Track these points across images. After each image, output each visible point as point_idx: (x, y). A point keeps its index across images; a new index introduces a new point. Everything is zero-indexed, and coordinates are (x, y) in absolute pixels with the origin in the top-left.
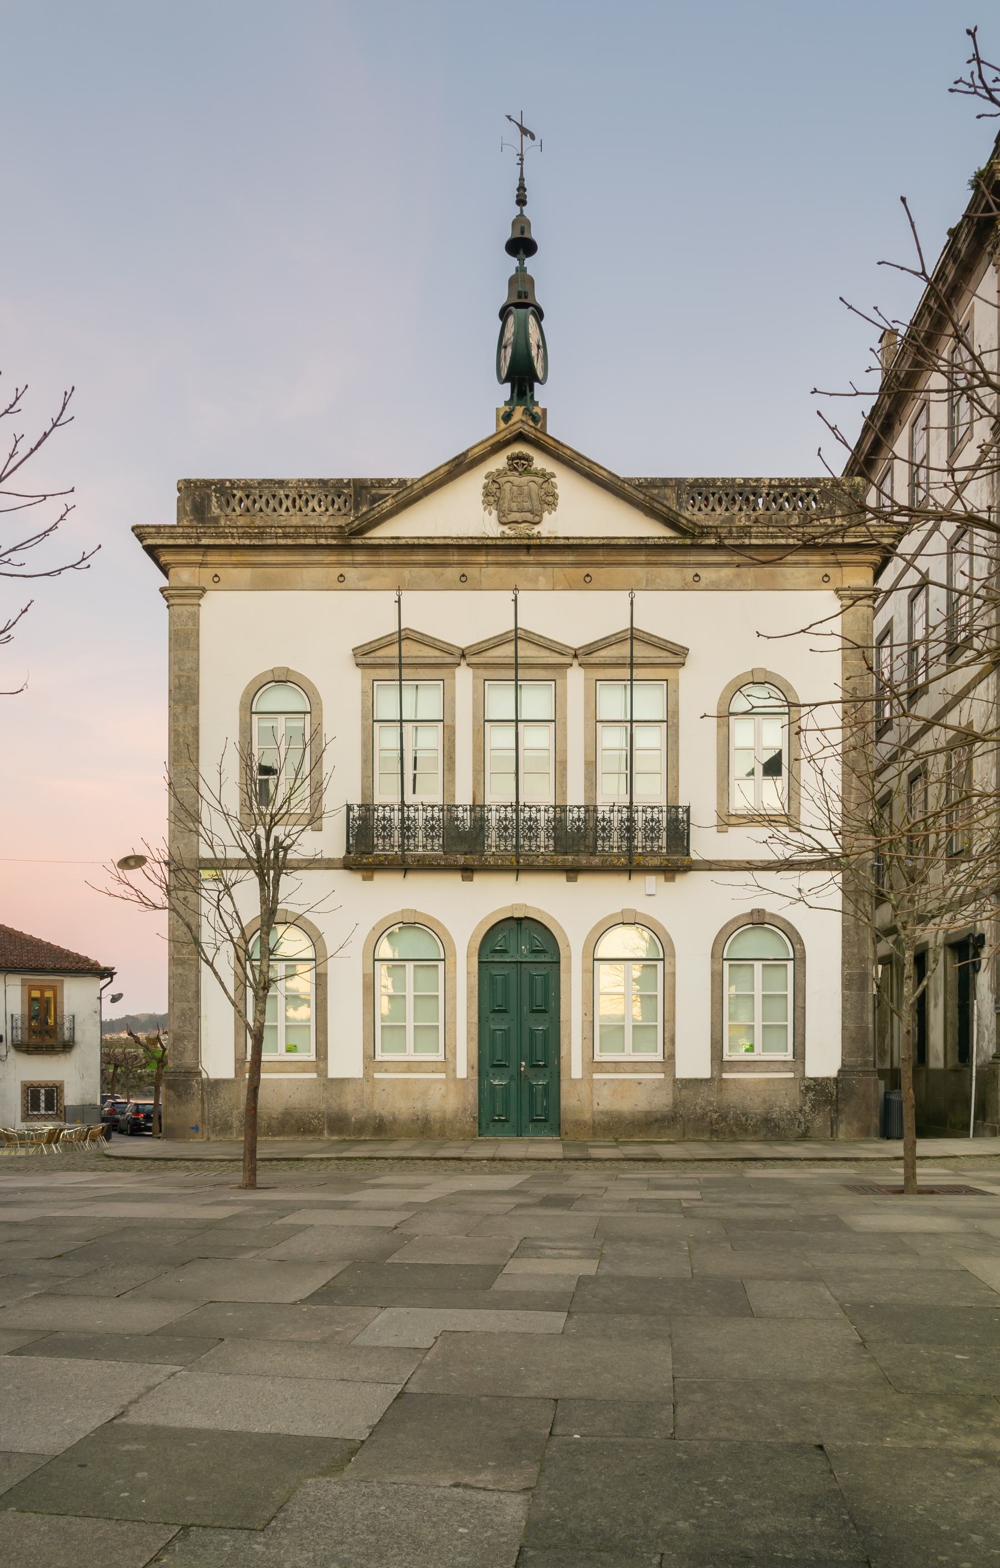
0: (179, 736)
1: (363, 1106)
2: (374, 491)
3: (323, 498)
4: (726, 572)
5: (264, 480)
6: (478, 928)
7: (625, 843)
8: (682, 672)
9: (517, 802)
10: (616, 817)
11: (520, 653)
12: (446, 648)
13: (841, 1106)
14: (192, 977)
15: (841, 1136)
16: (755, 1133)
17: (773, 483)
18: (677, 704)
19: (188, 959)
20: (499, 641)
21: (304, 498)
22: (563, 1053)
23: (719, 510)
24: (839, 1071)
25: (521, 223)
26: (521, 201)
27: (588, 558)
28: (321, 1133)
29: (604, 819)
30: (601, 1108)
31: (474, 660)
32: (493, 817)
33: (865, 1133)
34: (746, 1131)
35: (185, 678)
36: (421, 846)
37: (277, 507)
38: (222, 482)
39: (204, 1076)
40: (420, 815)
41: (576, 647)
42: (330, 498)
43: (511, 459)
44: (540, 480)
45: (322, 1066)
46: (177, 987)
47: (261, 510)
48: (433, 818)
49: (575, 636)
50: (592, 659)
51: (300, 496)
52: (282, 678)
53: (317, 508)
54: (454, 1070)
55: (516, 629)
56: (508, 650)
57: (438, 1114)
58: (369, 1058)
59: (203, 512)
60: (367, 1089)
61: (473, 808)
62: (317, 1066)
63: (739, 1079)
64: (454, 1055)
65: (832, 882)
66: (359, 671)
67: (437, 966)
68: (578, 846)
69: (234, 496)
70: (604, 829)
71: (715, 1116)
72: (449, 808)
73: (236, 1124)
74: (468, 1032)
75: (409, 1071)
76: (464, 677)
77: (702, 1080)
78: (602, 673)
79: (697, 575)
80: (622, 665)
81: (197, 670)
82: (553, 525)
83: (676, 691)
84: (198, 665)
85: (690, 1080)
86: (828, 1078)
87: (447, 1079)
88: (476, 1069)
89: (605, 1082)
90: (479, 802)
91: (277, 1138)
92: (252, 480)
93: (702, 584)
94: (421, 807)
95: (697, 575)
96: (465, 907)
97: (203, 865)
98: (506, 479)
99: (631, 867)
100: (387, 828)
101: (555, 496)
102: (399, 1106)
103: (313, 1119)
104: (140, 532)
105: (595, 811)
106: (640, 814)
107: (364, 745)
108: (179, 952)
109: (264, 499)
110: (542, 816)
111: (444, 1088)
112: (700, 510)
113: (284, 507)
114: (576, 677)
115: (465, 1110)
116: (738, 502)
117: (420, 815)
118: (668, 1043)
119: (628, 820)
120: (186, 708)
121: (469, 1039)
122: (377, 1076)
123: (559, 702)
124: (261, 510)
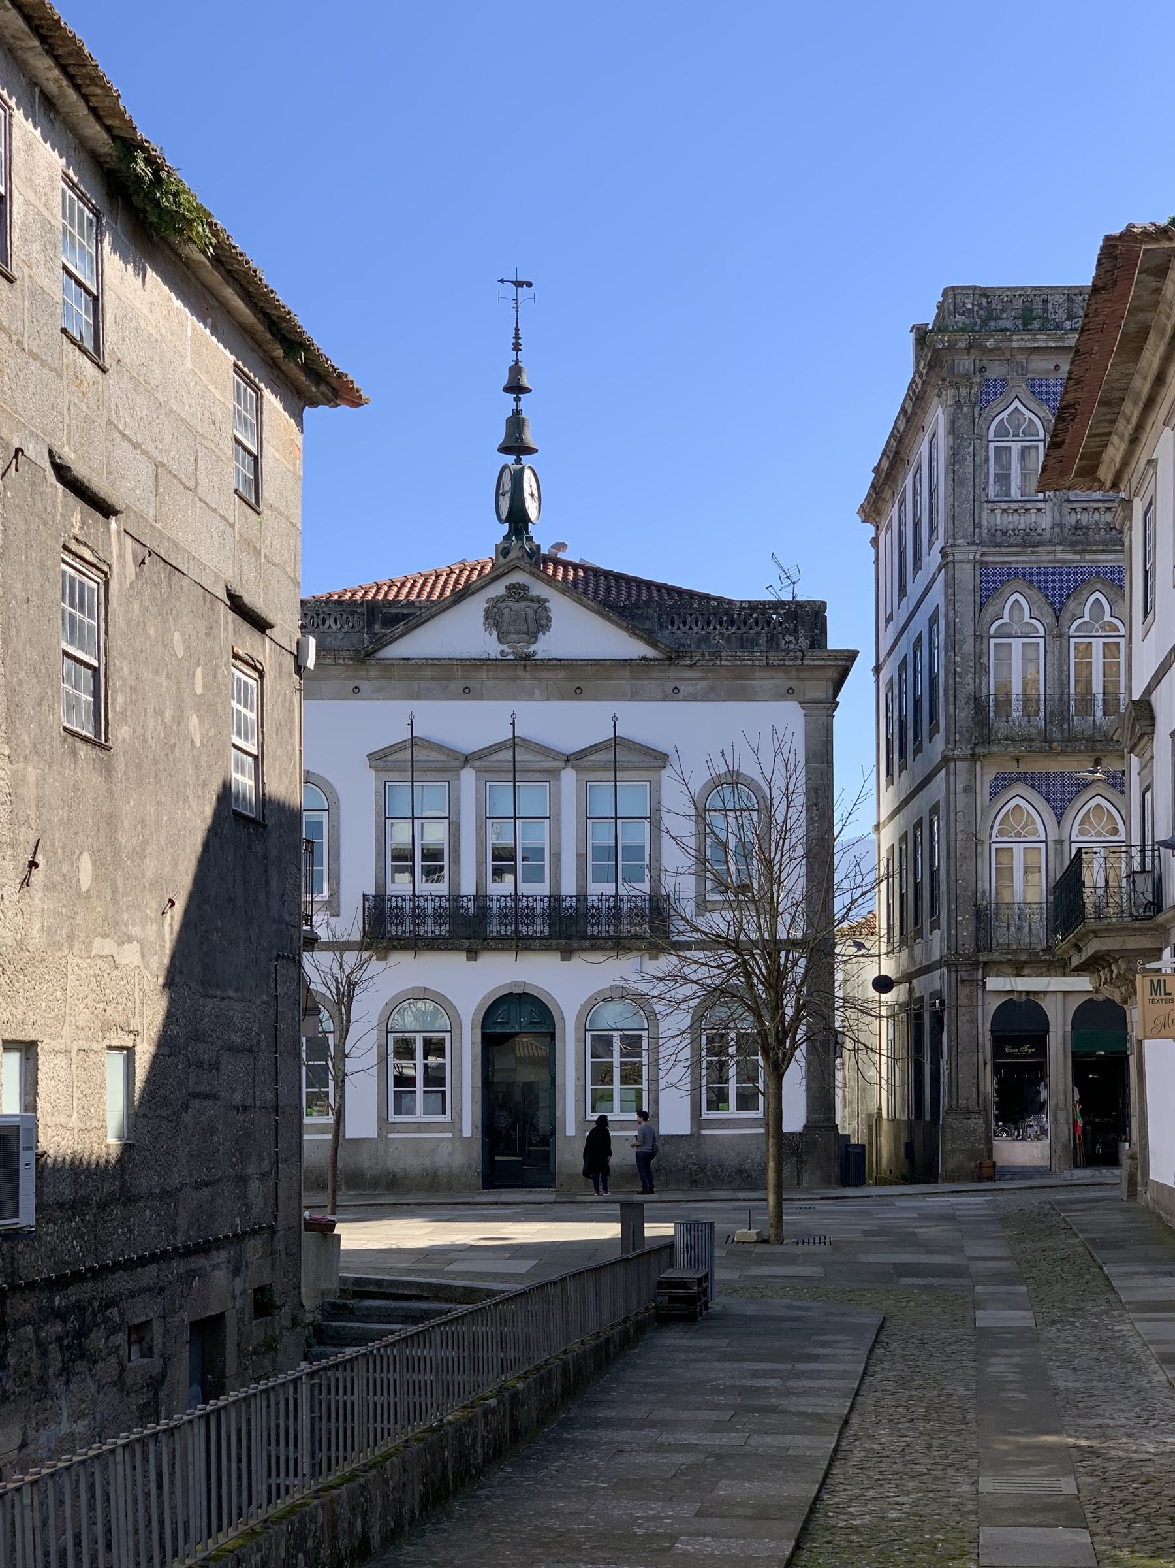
2: (385, 610)
4: (702, 685)
6: (481, 1004)
8: (664, 773)
9: (516, 894)
10: (604, 906)
11: (518, 758)
12: (452, 753)
13: (805, 1157)
15: (805, 1185)
16: (730, 1182)
21: (321, 616)
22: (558, 1114)
24: (805, 1127)
25: (516, 370)
26: (517, 348)
27: (579, 678)
29: (593, 907)
31: (477, 764)
33: (827, 1182)
34: (722, 1180)
36: (429, 929)
40: (429, 906)
42: (344, 617)
43: (508, 588)
44: (535, 605)
48: (440, 907)
50: (581, 764)
51: (318, 615)
53: (333, 626)
54: (461, 1130)
56: (507, 755)
58: (383, 1120)
61: (476, 898)
66: (373, 772)
67: (444, 1112)
70: (593, 916)
72: (455, 898)
74: (473, 1096)
76: (468, 777)
78: (590, 777)
82: (546, 646)
83: (658, 791)
85: (672, 1136)
90: (482, 893)
93: (681, 695)
96: (468, 984)
99: (618, 944)
101: (549, 619)
102: (411, 1163)
110: (538, 906)
111: (451, 1147)
114: (569, 777)
115: (470, 1166)
117: (429, 906)
118: (652, 1103)
121: (474, 1102)
122: (391, 1136)
123: (554, 800)
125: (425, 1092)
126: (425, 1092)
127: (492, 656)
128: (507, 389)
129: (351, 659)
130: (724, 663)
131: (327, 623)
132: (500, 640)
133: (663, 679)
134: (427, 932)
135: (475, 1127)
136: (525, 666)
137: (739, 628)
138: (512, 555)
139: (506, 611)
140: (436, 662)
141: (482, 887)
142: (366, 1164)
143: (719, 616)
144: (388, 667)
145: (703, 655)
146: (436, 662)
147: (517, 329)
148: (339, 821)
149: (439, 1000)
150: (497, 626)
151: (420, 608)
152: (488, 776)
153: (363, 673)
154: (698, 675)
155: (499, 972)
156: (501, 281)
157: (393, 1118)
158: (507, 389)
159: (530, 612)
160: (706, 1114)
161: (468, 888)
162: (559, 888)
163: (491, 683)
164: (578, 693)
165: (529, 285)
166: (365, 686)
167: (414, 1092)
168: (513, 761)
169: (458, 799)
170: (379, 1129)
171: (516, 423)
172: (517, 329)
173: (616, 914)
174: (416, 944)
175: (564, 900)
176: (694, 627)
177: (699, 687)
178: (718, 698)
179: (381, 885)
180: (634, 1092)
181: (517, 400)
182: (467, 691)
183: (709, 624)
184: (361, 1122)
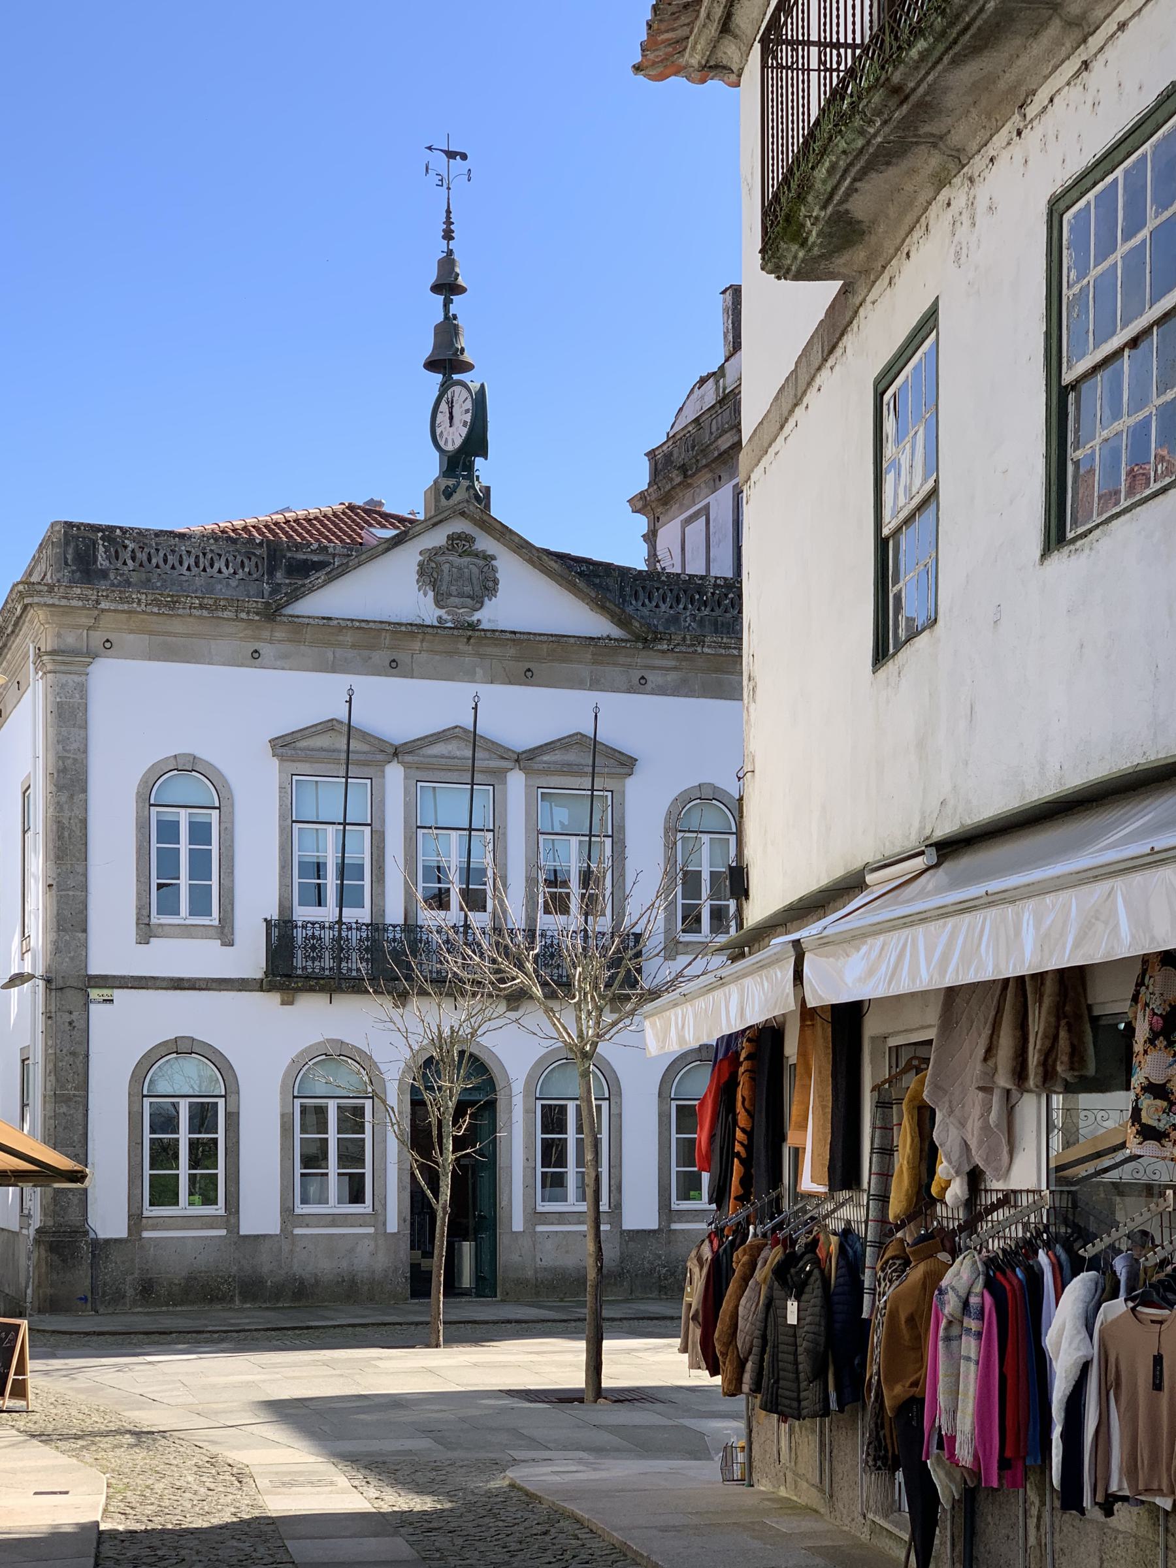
0: (63, 828)
2: (289, 555)
3: (231, 558)
4: (672, 677)
5: (161, 531)
8: (630, 782)
14: (80, 1116)
17: (718, 581)
18: (623, 818)
19: (74, 1095)
21: (209, 556)
25: (447, 263)
26: (448, 235)
27: (531, 658)
28: (232, 1300)
30: (544, 1263)
34: (885, 1235)
35: (69, 761)
37: (177, 564)
38: (112, 529)
39: (92, 1235)
41: (520, 750)
42: (239, 559)
44: (481, 563)
45: (233, 1221)
46: (60, 1129)
47: (157, 566)
49: (523, 738)
51: (204, 554)
52: (187, 766)
53: (224, 569)
54: (385, 1224)
57: (366, 1275)
58: (287, 1212)
59: (88, 564)
60: (286, 1247)
62: (228, 1221)
63: (688, 1230)
64: (384, 1206)
66: (276, 761)
69: (126, 547)
73: (130, 1292)
75: (333, 1224)
79: (643, 678)
80: (581, 774)
81: (85, 751)
84: (86, 745)
85: (638, 1231)
87: (376, 1233)
88: (408, 1222)
89: (549, 1235)
91: (179, 1308)
92: (147, 530)
94: (354, 926)
95: (643, 678)
96: (387, 1036)
97: (92, 984)
101: (496, 582)
102: (324, 1266)
103: (222, 1284)
106: (300, 930)
107: (282, 849)
108: (63, 1087)
109: (161, 554)
111: (372, 1243)
113: (186, 565)
114: (516, 781)
115: (396, 1269)
116: (683, 600)
120: (72, 796)
121: (401, 1189)
122: (297, 1231)
123: (378, 804)
124: (157, 566)
125: (339, 1174)
126: (302, 1175)
127: (428, 622)
128: (436, 289)
129: (257, 614)
130: (706, 650)
131: (216, 566)
132: (438, 603)
133: (630, 666)
134: (323, 969)
135: (402, 1219)
136: (469, 638)
137: (712, 610)
138: (457, 497)
139: (446, 567)
140: (363, 625)
141: (411, 915)
142: (265, 1269)
143: (690, 593)
144: (299, 626)
145: (684, 639)
146: (363, 625)
147: (448, 212)
148: (233, 823)
149: (364, 1060)
150: (434, 585)
151: (334, 555)
152: (420, 775)
153: (266, 634)
154: (673, 663)
155: (428, 1020)
156: (430, 148)
157: (301, 1209)
158: (436, 289)
159: (475, 570)
160: (677, 1205)
161: (394, 914)
162: (383, 916)
163: (424, 656)
164: (528, 677)
165: (464, 157)
166: (266, 649)
167: (327, 1174)
168: (471, 758)
169: (383, 802)
170: (283, 1222)
171: (448, 330)
172: (448, 212)
173: (340, 948)
174: (335, 984)
175: (385, 930)
176: (661, 604)
177: (669, 678)
178: (691, 694)
179: (285, 907)
181: (447, 304)
182: (394, 664)
183: (678, 602)
184: (260, 1214)
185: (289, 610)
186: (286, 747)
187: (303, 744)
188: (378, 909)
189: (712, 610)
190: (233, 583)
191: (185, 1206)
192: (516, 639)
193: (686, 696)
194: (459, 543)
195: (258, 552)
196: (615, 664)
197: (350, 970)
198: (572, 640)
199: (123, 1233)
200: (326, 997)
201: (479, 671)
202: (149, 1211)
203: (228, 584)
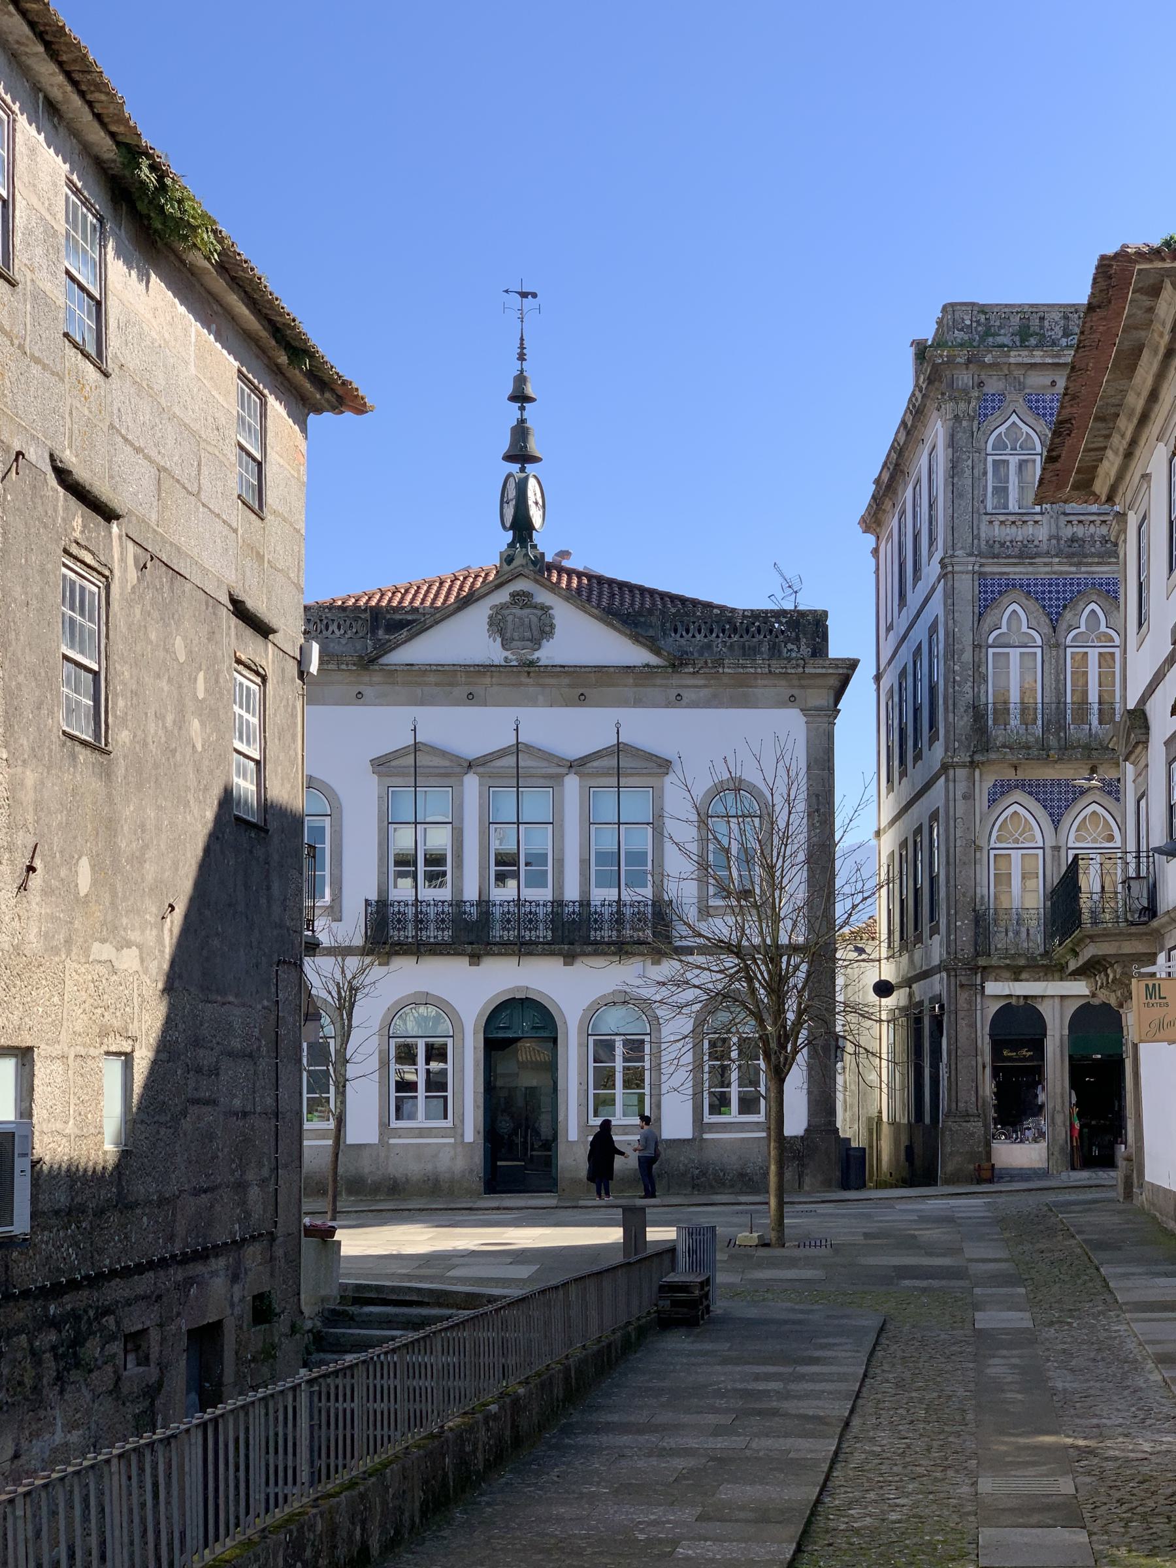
1: (378, 1169)
2: (388, 616)
6: (483, 1009)
7: (614, 933)
8: (668, 779)
10: (606, 911)
12: (455, 758)
15: (806, 1188)
16: (732, 1186)
20: (502, 753)
23: (698, 636)
25: (521, 380)
26: (522, 357)
27: (583, 684)
29: (596, 913)
31: (481, 770)
32: (497, 911)
33: (828, 1185)
34: (724, 1184)
36: (431, 934)
40: (432, 911)
41: (471, 758)
42: (348, 623)
43: (513, 595)
44: (539, 613)
48: (443, 913)
49: (575, 750)
53: (336, 631)
54: (463, 1136)
55: (518, 743)
58: (384, 1125)
60: (383, 1155)
61: (479, 903)
65: (866, 895)
66: (375, 777)
68: (572, 933)
70: (596, 921)
71: (697, 1172)
74: (475, 1101)
76: (471, 783)
77: (684, 1140)
80: (408, 775)
82: (550, 653)
85: (674, 1140)
86: (796, 1137)
96: (472, 988)
98: (508, 611)
99: (621, 949)
100: (401, 921)
101: (552, 626)
102: (413, 1168)
104: (366, 900)
105: (589, 904)
110: (541, 911)
111: (452, 1153)
112: (682, 636)
114: (572, 783)
115: (472, 1171)
117: (432, 911)
119: (616, 913)
121: (476, 1107)
122: (392, 1141)
125: (427, 1097)
128: (513, 398)
130: (726, 670)
133: (666, 686)
137: (741, 637)
138: (516, 563)
139: (510, 618)
140: (440, 668)
141: (485, 892)
142: (366, 1170)
144: (391, 673)
145: (706, 663)
147: (522, 339)
151: (424, 615)
154: (701, 682)
155: (502, 977)
156: (507, 291)
159: (534, 619)
160: (708, 1118)
162: (562, 894)
163: (496, 689)
164: (582, 700)
165: (534, 295)
166: (368, 691)
167: (416, 1097)
168: (517, 767)
171: (521, 432)
172: (522, 339)
174: (419, 949)
179: (383, 890)
180: (636, 1097)
182: (471, 697)
183: (711, 631)
184: (362, 1128)
185: (385, 660)
186: (381, 765)
187: (393, 763)
188: (458, 888)
189: (741, 637)
190: (343, 641)
191: (733, 1115)
192: (563, 670)
193: (716, 707)
194: (521, 599)
195: (363, 616)
196: (655, 686)
197: (602, 937)
198: (612, 669)
199: (375, 1140)
200: (414, 959)
201: (541, 698)
202: (708, 1118)
203: (339, 643)
